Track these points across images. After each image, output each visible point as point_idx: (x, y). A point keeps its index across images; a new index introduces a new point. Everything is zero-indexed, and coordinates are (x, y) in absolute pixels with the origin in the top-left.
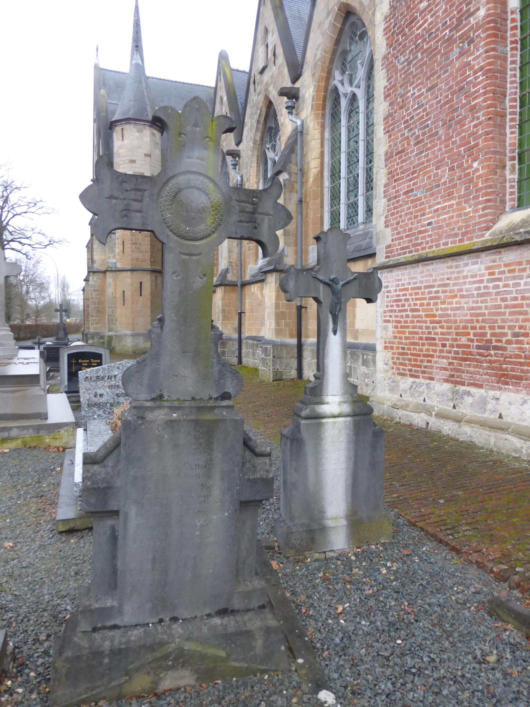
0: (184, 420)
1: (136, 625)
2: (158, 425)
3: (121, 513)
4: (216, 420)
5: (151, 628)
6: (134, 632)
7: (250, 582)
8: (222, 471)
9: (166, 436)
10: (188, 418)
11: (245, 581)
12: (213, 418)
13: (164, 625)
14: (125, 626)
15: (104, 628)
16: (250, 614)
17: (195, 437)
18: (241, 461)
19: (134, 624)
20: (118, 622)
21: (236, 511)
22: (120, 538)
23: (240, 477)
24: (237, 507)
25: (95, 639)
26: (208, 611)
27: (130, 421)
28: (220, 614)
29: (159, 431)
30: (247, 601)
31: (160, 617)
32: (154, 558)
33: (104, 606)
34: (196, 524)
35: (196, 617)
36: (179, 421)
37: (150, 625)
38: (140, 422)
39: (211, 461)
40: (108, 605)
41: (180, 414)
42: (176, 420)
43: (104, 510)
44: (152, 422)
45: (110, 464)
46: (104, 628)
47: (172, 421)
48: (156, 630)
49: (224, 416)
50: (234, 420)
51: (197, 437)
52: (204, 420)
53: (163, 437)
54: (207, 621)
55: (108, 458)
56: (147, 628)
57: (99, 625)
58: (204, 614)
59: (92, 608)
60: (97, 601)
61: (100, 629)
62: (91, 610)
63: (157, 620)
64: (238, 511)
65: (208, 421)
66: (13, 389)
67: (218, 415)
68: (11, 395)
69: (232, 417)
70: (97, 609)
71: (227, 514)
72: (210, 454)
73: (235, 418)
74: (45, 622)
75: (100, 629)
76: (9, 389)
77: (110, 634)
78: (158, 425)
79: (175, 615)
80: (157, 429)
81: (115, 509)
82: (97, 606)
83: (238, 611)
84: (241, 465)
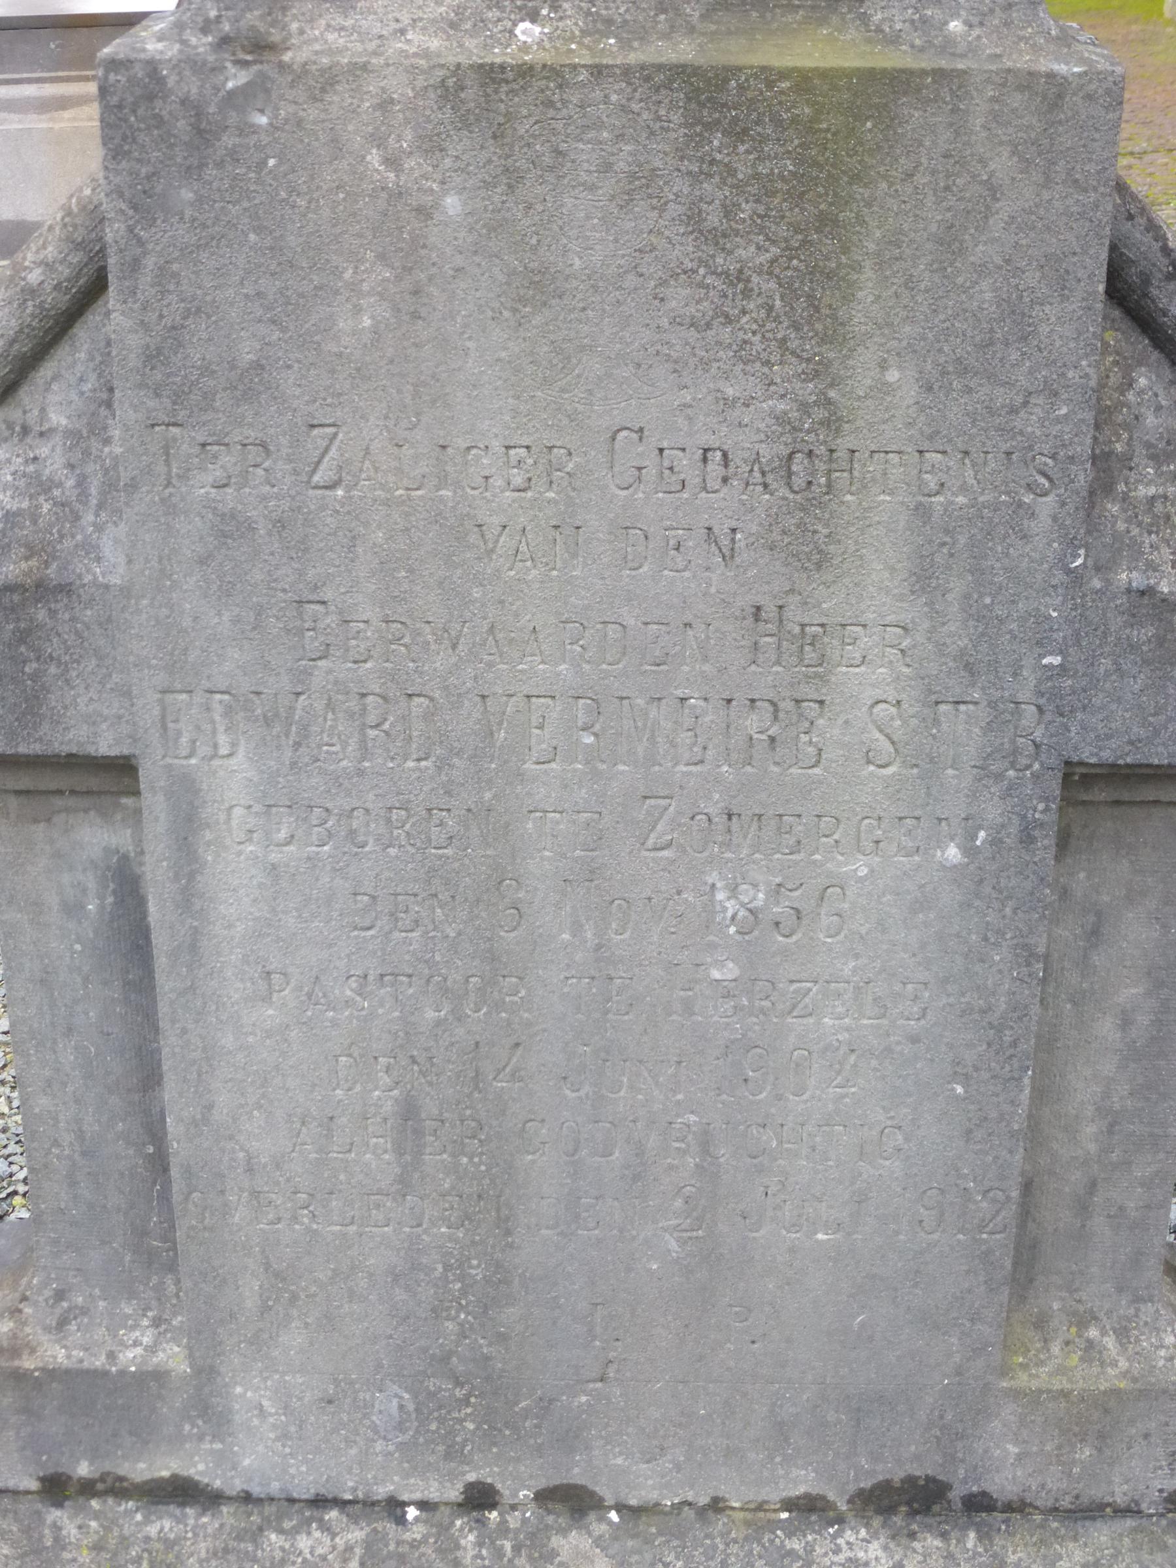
0: (598, 71)
1: (320, 1502)
2: (385, 104)
3: (148, 773)
4: (871, 76)
5: (417, 1532)
6: (303, 1543)
7: (1122, 1333)
8: (922, 512)
9: (452, 204)
10: (633, 58)
11: (1083, 1320)
12: (852, 61)
13: (503, 1529)
14: (247, 1498)
15: (118, 1488)
16: (1102, 1534)
17: (693, 219)
18: (1083, 447)
19: (304, 1492)
20: (199, 1469)
21: (1027, 838)
22: (160, 941)
23: (1076, 578)
24: (1044, 811)
25: (60, 1543)
26: (802, 1482)
27: (152, 66)
28: (888, 1511)
29: (392, 162)
30: (1085, 1453)
31: (472, 1477)
32: (409, 1111)
33: (100, 1362)
34: (710, 908)
35: (717, 1505)
36: (555, 72)
37: (412, 1513)
38: (236, 79)
39: (833, 423)
40: (130, 1357)
41: (573, 23)
42: (526, 71)
43: (23, 749)
44: (329, 79)
45: (58, 418)
46: (118, 1488)
47: (491, 74)
48: (449, 1548)
49: (948, 45)
50: (1027, 81)
51: (714, 219)
52: (769, 76)
53: (424, 213)
54: (795, 1544)
55: (46, 371)
56: (391, 1527)
57: (84, 1469)
58: (774, 1495)
59: (28, 1363)
60: (62, 1323)
61: (88, 1488)
62: (19, 1377)
63: (454, 1493)
64: (1046, 842)
65: (804, 80)
66: (49, 90)
67: (894, 40)
68: (39, 123)
69: (1022, 60)
70: (53, 1374)
71: (953, 853)
72: (818, 371)
73: (1047, 64)
74: (1014, 1044)
75: (88, 1488)
76: (30, 90)
77: (153, 1530)
78: (385, 104)
79: (577, 1476)
80: (377, 139)
81: (106, 746)
82: (57, 1354)
83: (1018, 1507)
84: (1083, 476)
